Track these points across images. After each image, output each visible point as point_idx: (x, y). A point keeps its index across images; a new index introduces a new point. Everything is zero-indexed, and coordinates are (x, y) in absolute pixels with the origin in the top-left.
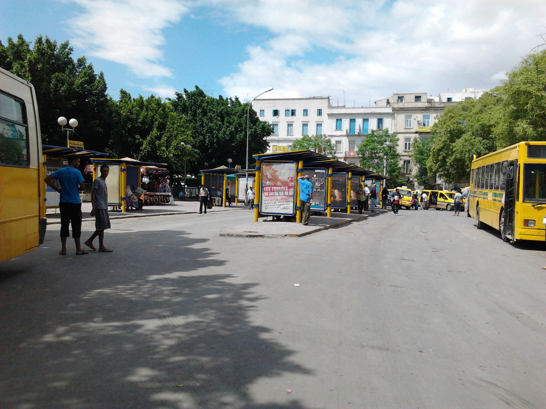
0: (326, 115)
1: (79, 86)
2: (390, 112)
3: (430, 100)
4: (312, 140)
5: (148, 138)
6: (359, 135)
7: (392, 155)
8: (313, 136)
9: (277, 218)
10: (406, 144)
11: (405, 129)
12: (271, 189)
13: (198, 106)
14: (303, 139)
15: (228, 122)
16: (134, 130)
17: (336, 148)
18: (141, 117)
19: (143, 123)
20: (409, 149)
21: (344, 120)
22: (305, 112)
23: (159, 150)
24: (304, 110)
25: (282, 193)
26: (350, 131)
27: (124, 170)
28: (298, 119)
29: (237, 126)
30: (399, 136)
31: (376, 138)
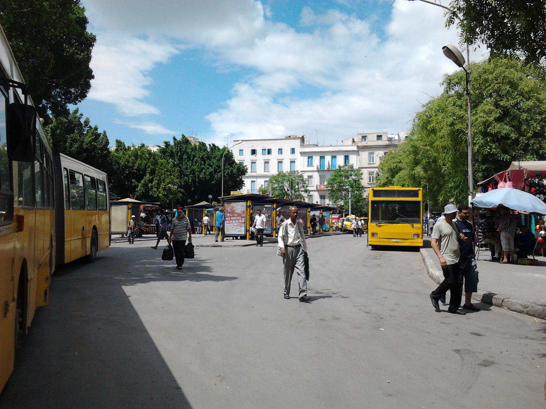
0: (299, 153)
1: (89, 143)
2: (355, 150)
3: (390, 138)
4: (286, 176)
5: (143, 182)
6: (328, 170)
7: (356, 188)
8: (287, 172)
9: (236, 237)
10: (370, 178)
11: (369, 164)
12: (230, 219)
13: (183, 152)
14: (278, 175)
15: (209, 165)
16: (132, 175)
17: (308, 183)
18: (136, 165)
19: (138, 169)
20: (373, 181)
21: (315, 157)
22: (280, 151)
23: (151, 190)
24: (279, 149)
25: (237, 221)
26: (320, 167)
27: (131, 208)
28: (274, 158)
29: (216, 168)
30: (363, 171)
31: (342, 173)
